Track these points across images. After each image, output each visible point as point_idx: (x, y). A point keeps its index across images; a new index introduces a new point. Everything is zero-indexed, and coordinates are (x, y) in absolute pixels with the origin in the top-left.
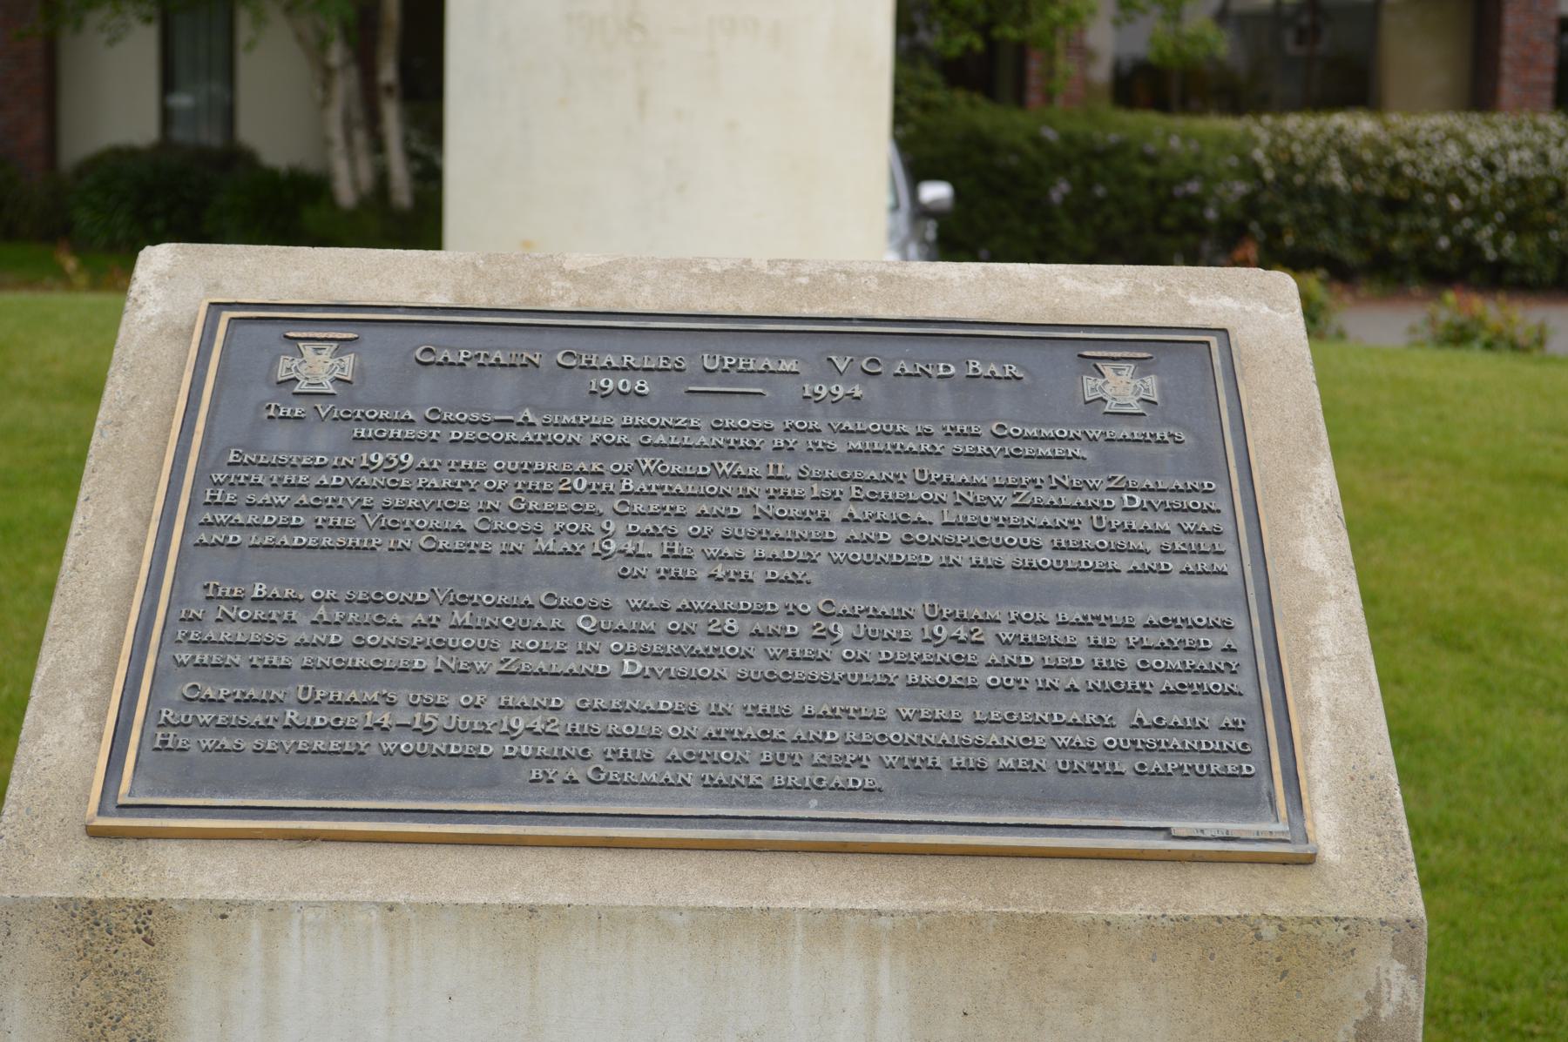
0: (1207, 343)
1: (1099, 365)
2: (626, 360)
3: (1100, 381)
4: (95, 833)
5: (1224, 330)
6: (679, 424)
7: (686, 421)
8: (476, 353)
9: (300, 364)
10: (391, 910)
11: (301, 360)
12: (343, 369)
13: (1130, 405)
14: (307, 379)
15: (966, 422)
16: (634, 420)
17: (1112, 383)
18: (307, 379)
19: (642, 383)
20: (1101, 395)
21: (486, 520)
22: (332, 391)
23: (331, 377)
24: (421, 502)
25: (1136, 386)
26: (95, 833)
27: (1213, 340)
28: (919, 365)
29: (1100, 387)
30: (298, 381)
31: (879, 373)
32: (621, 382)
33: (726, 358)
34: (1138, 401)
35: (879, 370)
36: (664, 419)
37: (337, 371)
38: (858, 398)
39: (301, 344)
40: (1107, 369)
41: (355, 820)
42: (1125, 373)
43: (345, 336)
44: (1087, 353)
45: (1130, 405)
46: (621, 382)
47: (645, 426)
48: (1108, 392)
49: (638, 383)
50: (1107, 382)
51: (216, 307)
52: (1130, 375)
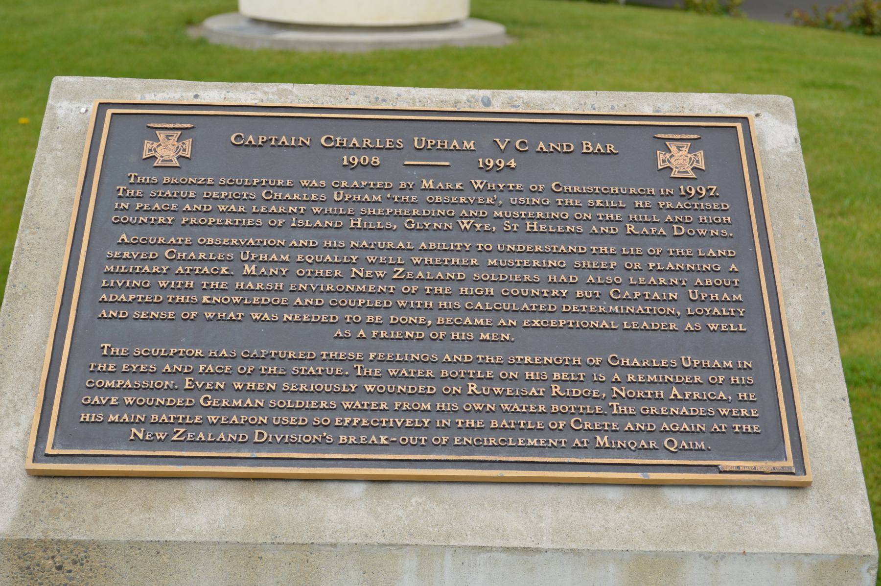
0: (735, 127)
1: (667, 143)
2: (608, 148)
3: (668, 155)
4: (40, 476)
5: (746, 118)
6: (200, 182)
7: (205, 180)
8: (270, 137)
9: (158, 147)
10: (593, 554)
11: (158, 144)
12: (184, 150)
13: (687, 172)
14: (162, 157)
15: (619, 186)
16: (171, 180)
17: (676, 157)
18: (162, 157)
19: (376, 159)
20: (669, 165)
21: (173, 251)
22: (178, 165)
23: (692, 167)
24: (239, 241)
25: (178, 147)
26: (40, 476)
27: (739, 126)
28: (552, 145)
29: (155, 149)
30: (157, 158)
31: (527, 151)
32: (364, 158)
33: (429, 141)
34: (692, 169)
35: (527, 148)
36: (191, 179)
37: (181, 152)
38: (513, 168)
39: (157, 132)
40: (673, 147)
41: (107, 463)
42: (684, 149)
43: (185, 126)
44: (152, 125)
45: (687, 172)
46: (364, 158)
47: (178, 184)
48: (674, 163)
49: (373, 159)
50: (672, 156)
51: (103, 106)
52: (176, 139)
